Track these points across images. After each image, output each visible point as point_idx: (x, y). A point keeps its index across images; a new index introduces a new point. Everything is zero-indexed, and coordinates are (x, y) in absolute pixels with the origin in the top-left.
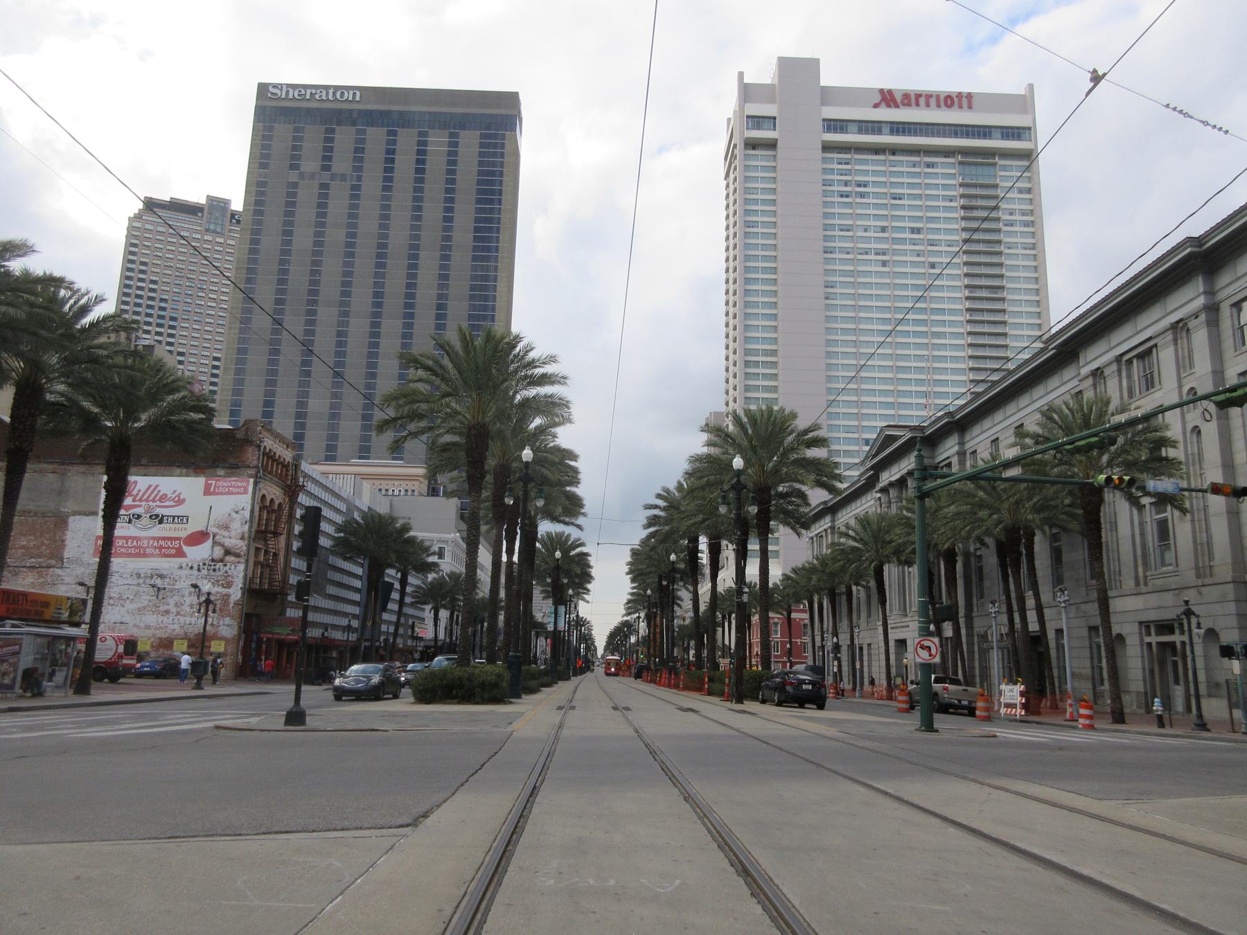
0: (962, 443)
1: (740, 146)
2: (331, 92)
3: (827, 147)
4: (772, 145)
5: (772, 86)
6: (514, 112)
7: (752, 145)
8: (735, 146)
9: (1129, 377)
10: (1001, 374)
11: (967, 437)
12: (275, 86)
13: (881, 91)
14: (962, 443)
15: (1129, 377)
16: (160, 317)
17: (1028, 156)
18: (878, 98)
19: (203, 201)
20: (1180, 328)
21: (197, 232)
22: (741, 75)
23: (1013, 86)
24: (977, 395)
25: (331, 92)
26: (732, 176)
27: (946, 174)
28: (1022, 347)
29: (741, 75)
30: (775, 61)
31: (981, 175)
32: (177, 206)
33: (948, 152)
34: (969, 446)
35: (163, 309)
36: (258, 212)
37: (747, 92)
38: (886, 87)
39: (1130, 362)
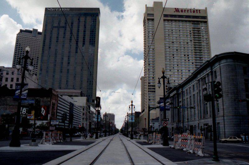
0: (212, 69)
1: (146, 20)
2: (63, 9)
3: (164, 20)
4: (153, 20)
5: (153, 7)
6: (99, 12)
7: (148, 19)
8: (145, 20)
9: (203, 81)
10: (199, 66)
11: (213, 67)
12: (49, 8)
13: (175, 8)
14: (212, 69)
15: (203, 81)
16: (19, 47)
17: (206, 22)
18: (175, 10)
19: (32, 30)
20: (208, 74)
21: (31, 37)
22: (146, 5)
23: (202, 8)
24: (198, 68)
25: (63, 9)
26: (145, 26)
27: (189, 27)
28: (205, 59)
29: (146, 5)
30: (153, 3)
31: (196, 26)
32: (27, 31)
33: (190, 21)
34: (214, 70)
35: (22, 50)
36: (45, 33)
37: (147, 8)
38: (177, 7)
39: (203, 79)
